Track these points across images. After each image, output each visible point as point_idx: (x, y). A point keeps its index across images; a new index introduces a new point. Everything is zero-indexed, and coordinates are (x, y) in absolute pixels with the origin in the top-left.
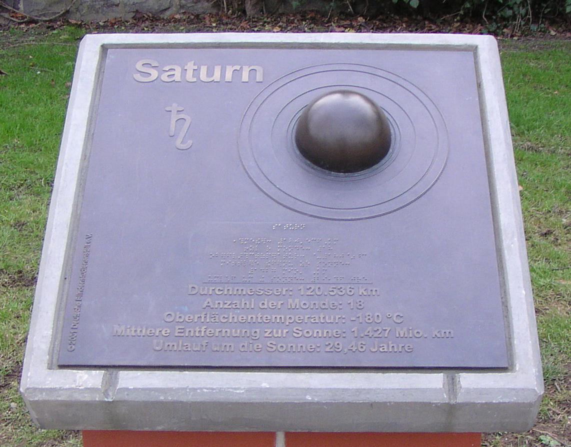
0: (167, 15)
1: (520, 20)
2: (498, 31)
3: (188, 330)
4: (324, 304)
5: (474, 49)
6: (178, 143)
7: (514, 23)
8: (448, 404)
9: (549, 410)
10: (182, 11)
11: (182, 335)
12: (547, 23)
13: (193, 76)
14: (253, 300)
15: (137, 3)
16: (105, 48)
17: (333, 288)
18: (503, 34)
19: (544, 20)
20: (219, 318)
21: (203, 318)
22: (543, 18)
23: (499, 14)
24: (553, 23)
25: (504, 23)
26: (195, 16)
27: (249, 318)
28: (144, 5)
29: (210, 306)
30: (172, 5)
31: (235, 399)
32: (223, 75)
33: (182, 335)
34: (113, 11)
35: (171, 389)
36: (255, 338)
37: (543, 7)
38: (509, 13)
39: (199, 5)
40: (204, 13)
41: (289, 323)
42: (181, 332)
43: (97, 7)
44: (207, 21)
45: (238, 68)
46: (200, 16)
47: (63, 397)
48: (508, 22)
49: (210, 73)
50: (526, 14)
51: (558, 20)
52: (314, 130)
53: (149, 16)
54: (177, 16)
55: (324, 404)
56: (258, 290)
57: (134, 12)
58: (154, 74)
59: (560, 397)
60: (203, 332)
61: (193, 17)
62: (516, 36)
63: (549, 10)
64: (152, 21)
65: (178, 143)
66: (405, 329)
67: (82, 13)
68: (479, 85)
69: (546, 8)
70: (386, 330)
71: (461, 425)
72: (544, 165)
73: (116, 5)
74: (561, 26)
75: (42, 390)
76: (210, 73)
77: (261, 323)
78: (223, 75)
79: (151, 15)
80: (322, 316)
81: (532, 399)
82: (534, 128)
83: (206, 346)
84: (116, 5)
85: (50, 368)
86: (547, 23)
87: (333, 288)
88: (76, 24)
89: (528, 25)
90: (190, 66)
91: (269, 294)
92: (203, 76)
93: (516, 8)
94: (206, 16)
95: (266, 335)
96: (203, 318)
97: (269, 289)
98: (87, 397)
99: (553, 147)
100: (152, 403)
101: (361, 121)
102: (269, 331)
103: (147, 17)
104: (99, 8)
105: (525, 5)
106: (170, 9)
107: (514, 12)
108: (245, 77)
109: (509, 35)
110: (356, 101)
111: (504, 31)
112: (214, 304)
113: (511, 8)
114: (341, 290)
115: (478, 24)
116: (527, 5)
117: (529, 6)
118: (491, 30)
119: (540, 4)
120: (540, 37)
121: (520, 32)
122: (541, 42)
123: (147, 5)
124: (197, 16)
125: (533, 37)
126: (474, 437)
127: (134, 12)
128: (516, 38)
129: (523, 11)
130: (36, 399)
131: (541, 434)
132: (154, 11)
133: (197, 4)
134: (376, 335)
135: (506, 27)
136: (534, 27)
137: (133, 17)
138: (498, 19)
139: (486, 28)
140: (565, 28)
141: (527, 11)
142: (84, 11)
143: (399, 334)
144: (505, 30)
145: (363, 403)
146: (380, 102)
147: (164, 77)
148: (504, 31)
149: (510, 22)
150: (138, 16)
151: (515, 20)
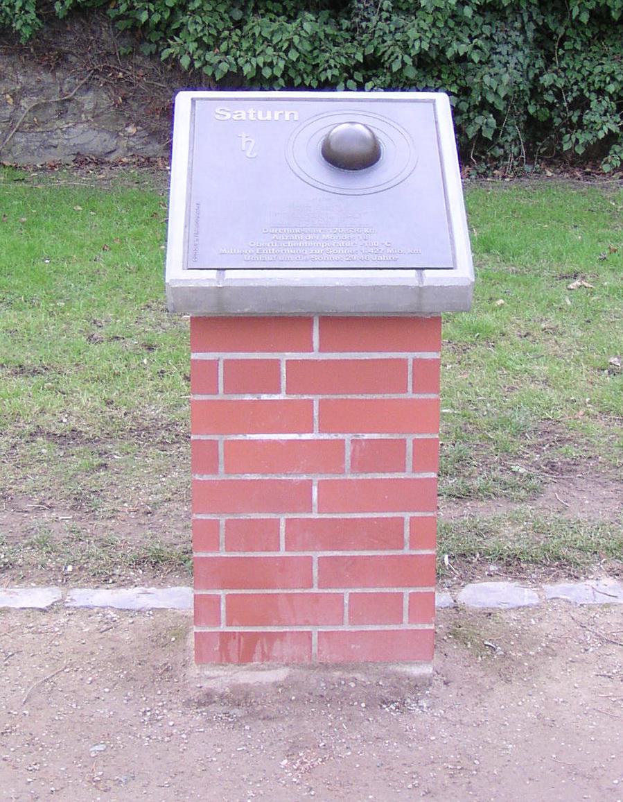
0: (112, 158)
1: (512, 159)
2: (487, 172)
5: (433, 101)
6: (248, 154)
7: (505, 163)
8: (418, 287)
9: (519, 450)
10: (130, 154)
12: (543, 163)
13: (254, 117)
15: (78, 144)
16: (193, 100)
18: (493, 175)
19: (540, 160)
22: (538, 158)
23: (489, 153)
24: (550, 164)
25: (495, 163)
26: (146, 159)
28: (86, 146)
30: (119, 147)
31: (294, 284)
32: (273, 116)
34: (50, 153)
35: (257, 279)
37: (538, 146)
38: (500, 152)
39: (150, 147)
40: (155, 156)
43: (33, 148)
44: (160, 164)
45: (282, 112)
46: (151, 159)
47: (193, 285)
48: (499, 162)
49: (264, 115)
50: (519, 153)
51: (556, 161)
52: (333, 147)
53: (92, 159)
54: (125, 160)
55: (347, 287)
57: (74, 154)
58: (228, 116)
59: (528, 442)
61: (143, 160)
62: (508, 177)
63: (545, 149)
64: (97, 164)
65: (248, 154)
67: (15, 155)
68: (436, 123)
69: (542, 147)
72: (526, 284)
73: (54, 147)
74: (559, 167)
75: (180, 281)
76: (264, 115)
78: (273, 116)
79: (94, 158)
81: (468, 283)
82: (519, 254)
84: (54, 147)
85: (183, 269)
86: (543, 163)
88: (11, 166)
89: (521, 166)
90: (251, 111)
92: (260, 117)
93: (507, 147)
94: (158, 160)
98: (207, 285)
99: (538, 271)
100: (246, 287)
101: (363, 140)
103: (89, 160)
104: (35, 150)
105: (518, 143)
106: (116, 152)
107: (505, 152)
108: (287, 117)
109: (500, 176)
110: (360, 128)
111: (495, 172)
113: (502, 147)
115: (465, 166)
116: (520, 144)
117: (522, 143)
118: (480, 172)
119: (534, 143)
120: (535, 179)
121: (512, 173)
122: (536, 182)
123: (90, 147)
124: (148, 159)
125: (528, 178)
127: (74, 154)
128: (507, 180)
129: (515, 150)
130: (176, 286)
131: (511, 465)
132: (97, 153)
133: (147, 146)
134: (375, 252)
135: (496, 168)
136: (528, 168)
137: (73, 161)
138: (488, 160)
139: (475, 169)
140: (563, 169)
141: (520, 150)
142: (17, 153)
144: (496, 172)
145: (370, 287)
146: (377, 133)
147: (235, 117)
148: (495, 172)
149: (501, 162)
150: (80, 159)
151: (507, 161)
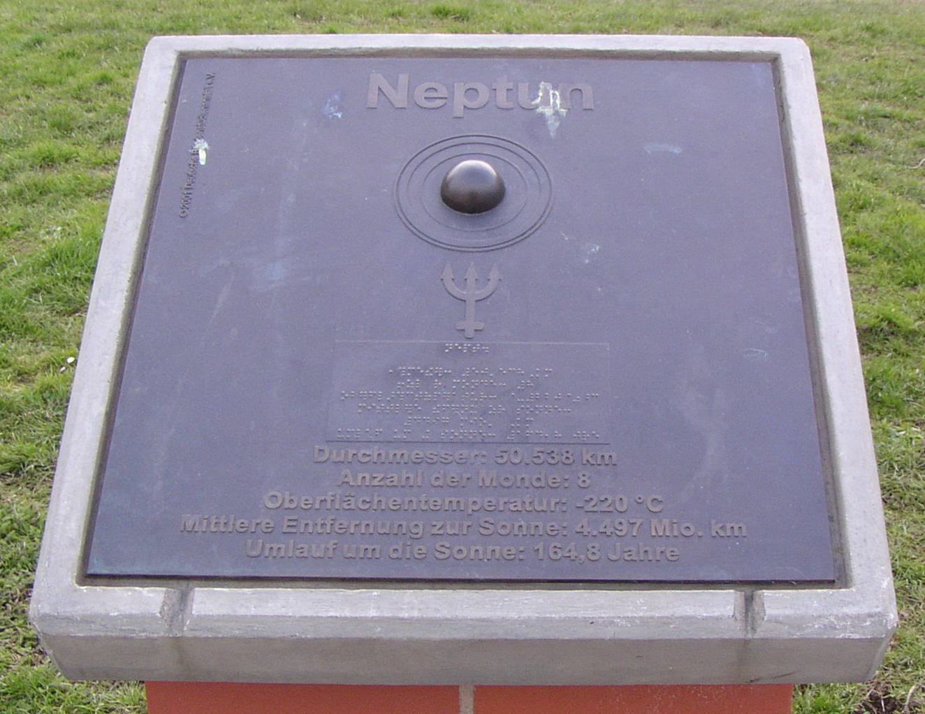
3: (304, 522)
4: (539, 479)
11: (294, 530)
14: (420, 472)
16: (184, 59)
17: (502, 452)
20: (356, 501)
21: (329, 501)
27: (447, 502)
29: (348, 483)
33: (294, 530)
36: (415, 536)
41: (473, 510)
42: (292, 526)
56: (443, 456)
60: (328, 526)
66: (666, 521)
70: (635, 523)
71: (765, 672)
77: (426, 510)
80: (527, 500)
83: (334, 549)
87: (502, 452)
90: (502, 85)
91: (447, 461)
95: (435, 531)
96: (329, 501)
97: (446, 454)
102: (439, 525)
112: (355, 479)
114: (552, 455)
126: (781, 692)
143: (656, 531)
